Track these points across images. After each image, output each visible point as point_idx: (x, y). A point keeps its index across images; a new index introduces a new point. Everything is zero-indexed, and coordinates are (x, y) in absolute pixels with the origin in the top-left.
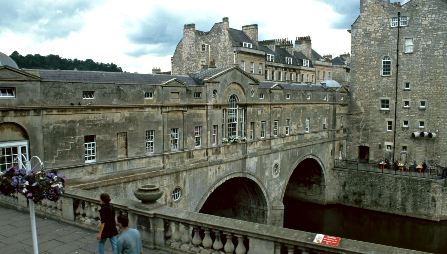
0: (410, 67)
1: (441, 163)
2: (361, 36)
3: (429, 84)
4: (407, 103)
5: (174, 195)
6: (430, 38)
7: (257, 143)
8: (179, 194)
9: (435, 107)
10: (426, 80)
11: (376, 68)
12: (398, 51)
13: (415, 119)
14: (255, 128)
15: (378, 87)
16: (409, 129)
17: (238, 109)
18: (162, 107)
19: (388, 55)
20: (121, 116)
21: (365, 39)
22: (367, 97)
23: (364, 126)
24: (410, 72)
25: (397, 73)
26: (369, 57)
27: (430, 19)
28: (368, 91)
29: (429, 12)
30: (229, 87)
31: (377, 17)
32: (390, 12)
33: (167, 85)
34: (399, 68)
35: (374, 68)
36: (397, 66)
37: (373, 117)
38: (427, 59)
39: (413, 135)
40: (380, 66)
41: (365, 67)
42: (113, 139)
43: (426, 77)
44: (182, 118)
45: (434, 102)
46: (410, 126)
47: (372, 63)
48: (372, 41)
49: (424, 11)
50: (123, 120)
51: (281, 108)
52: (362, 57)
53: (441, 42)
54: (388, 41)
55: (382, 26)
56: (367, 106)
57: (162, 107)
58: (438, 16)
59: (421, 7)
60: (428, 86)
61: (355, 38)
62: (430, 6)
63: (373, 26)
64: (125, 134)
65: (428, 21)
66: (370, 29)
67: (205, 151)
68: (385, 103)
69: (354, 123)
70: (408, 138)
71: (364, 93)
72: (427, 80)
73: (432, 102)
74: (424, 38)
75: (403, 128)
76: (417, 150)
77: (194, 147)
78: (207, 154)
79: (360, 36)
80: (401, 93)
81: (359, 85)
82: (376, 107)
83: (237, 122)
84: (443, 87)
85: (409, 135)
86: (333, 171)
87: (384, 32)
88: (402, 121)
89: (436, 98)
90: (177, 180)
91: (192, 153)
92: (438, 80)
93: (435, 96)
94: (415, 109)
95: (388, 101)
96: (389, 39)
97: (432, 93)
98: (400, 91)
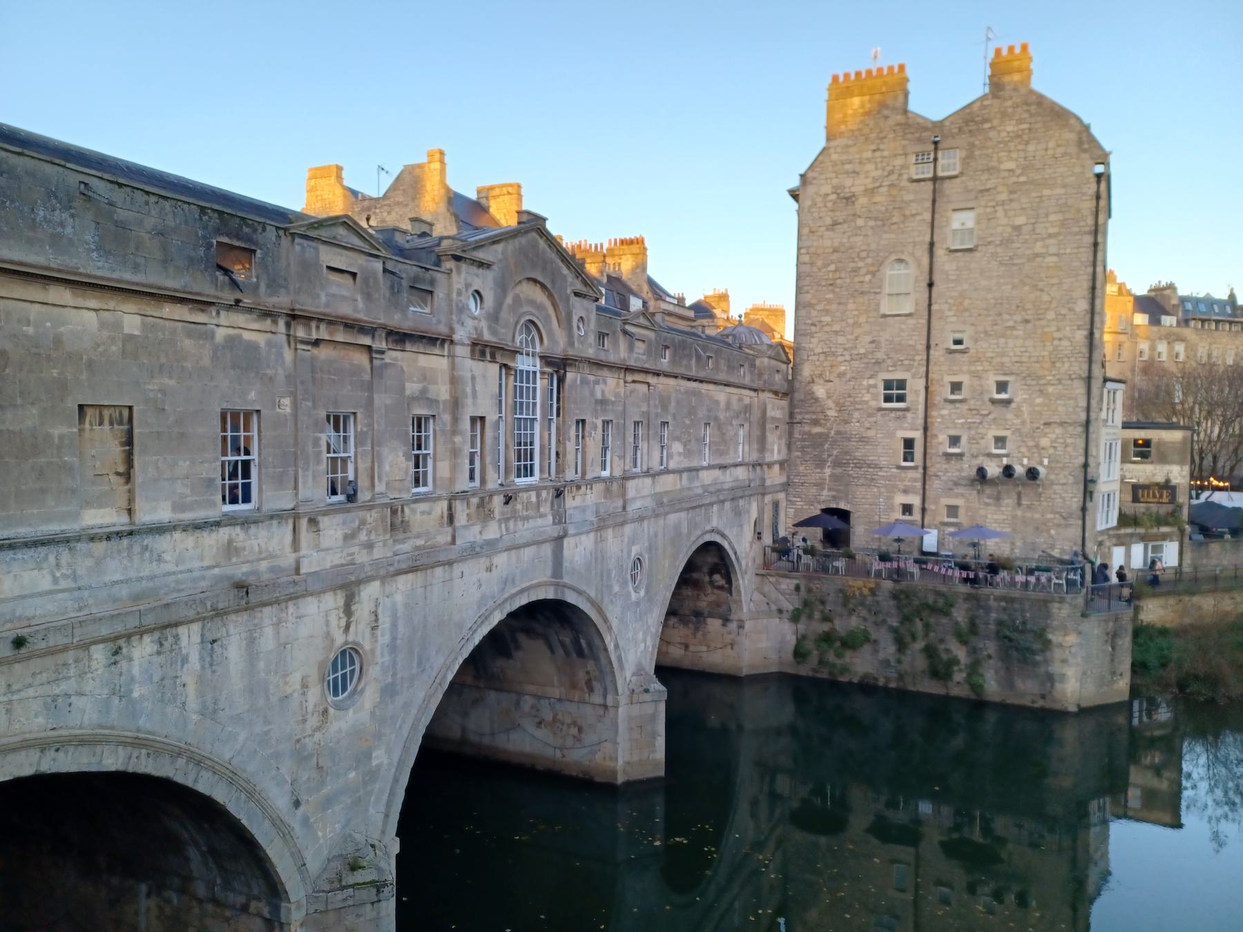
0: (966, 286)
1: (1057, 550)
2: (830, 205)
3: (1021, 333)
4: (956, 387)
5: (335, 680)
6: (1024, 206)
7: (591, 489)
8: (352, 672)
9: (1039, 397)
10: (1011, 323)
11: (869, 292)
12: (932, 244)
13: (980, 431)
14: (587, 439)
15: (874, 345)
16: (965, 458)
17: (543, 373)
18: (294, 317)
19: (903, 257)
20: (103, 325)
21: (838, 213)
22: (841, 375)
23: (835, 452)
24: (967, 302)
25: (930, 305)
26: (852, 265)
27: (1022, 154)
28: (848, 358)
29: (1019, 136)
30: (517, 290)
31: (874, 151)
32: (909, 136)
33: (311, 234)
34: (935, 289)
35: (862, 293)
36: (931, 285)
37: (862, 429)
38: (1013, 264)
39: (981, 472)
40: (880, 287)
41: (837, 290)
42: (56, 432)
43: (1010, 314)
44: (367, 377)
45: (1034, 383)
46: (966, 451)
47: (857, 279)
48: (860, 217)
49: (1004, 134)
50: (114, 348)
51: (648, 384)
52: (829, 265)
53: (1053, 218)
54: (904, 216)
55: (887, 176)
56: (845, 398)
57: (294, 317)
58: (1043, 146)
59: (995, 122)
60: (1017, 337)
61: (809, 211)
62: (1020, 121)
63: (862, 176)
64: (126, 419)
65: (1016, 160)
66: (853, 185)
67: (445, 504)
68: (895, 391)
69: (807, 447)
70: (964, 482)
71: (834, 363)
72: (1015, 322)
73: (1028, 383)
74: (1007, 207)
75: (948, 456)
76: (990, 516)
77: (408, 491)
78: (451, 518)
79: (825, 206)
80: (942, 359)
81: (820, 341)
82: (867, 402)
83: (538, 416)
84: (1060, 339)
85: (964, 474)
86: (759, 578)
87: (894, 192)
88: (943, 438)
89: (1041, 373)
90: (348, 611)
91: (403, 511)
92: (1043, 323)
93: (1037, 365)
94: (979, 403)
95: (902, 384)
96: (907, 213)
97: (1030, 357)
98: (937, 353)
